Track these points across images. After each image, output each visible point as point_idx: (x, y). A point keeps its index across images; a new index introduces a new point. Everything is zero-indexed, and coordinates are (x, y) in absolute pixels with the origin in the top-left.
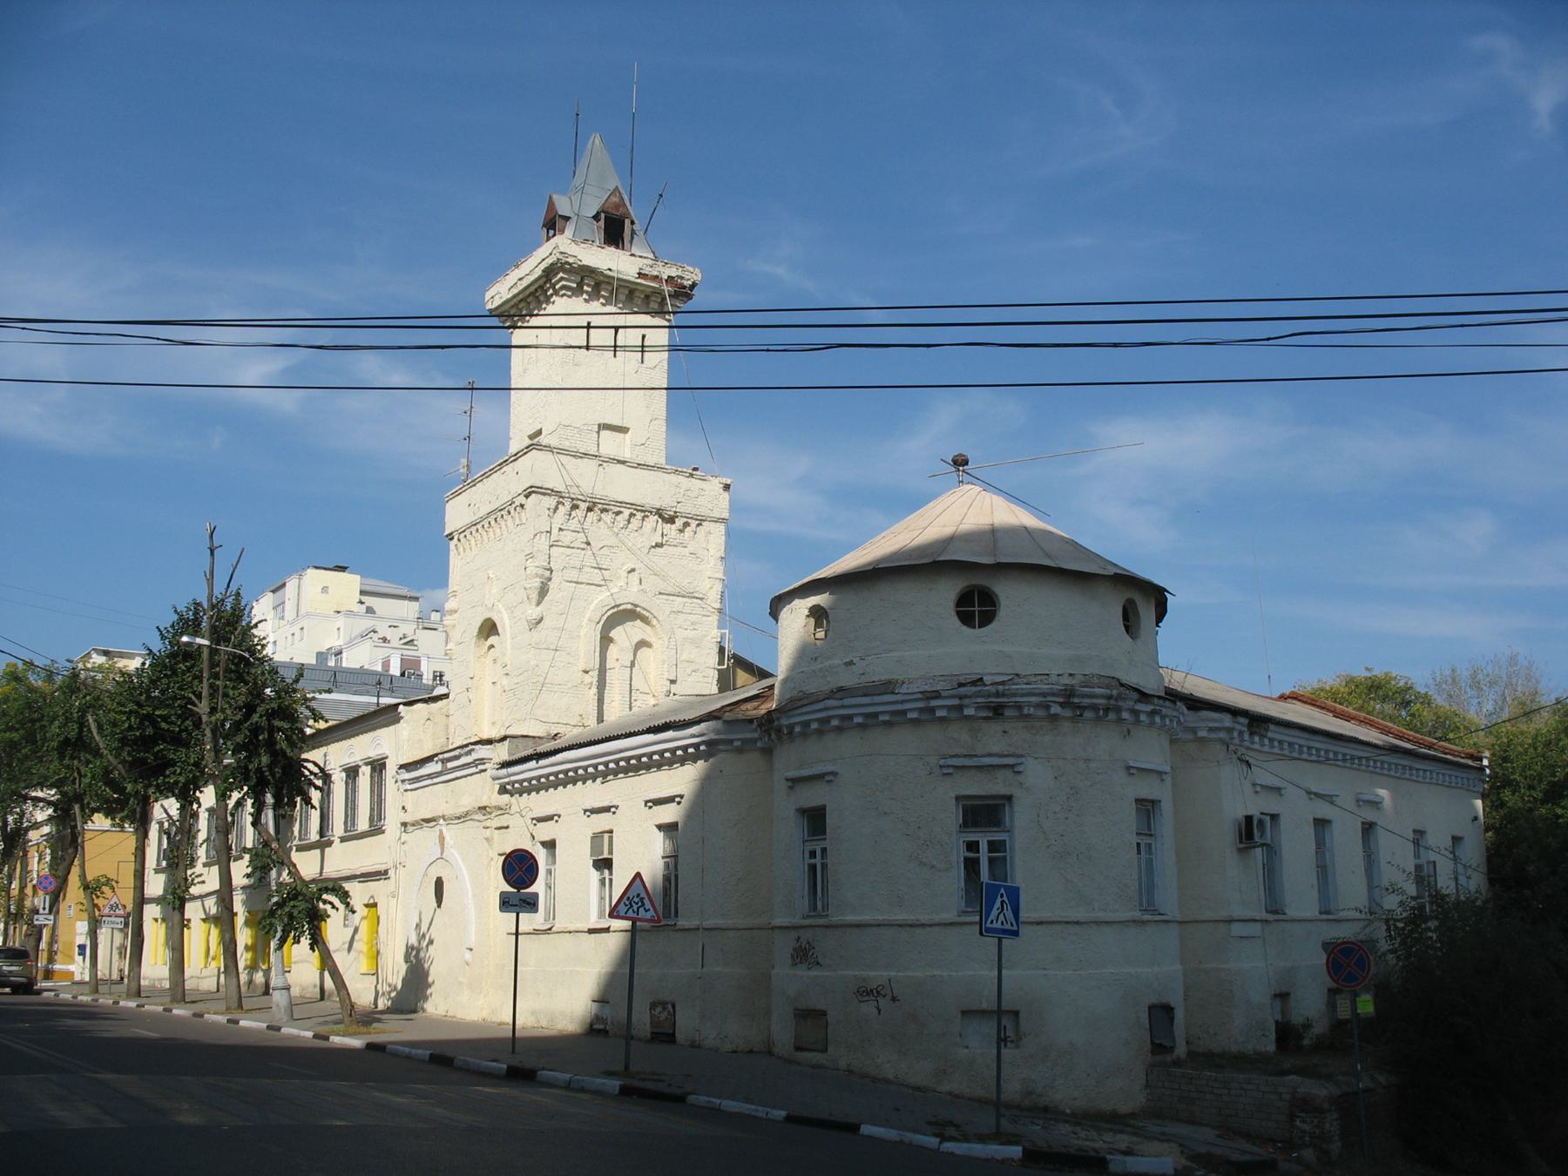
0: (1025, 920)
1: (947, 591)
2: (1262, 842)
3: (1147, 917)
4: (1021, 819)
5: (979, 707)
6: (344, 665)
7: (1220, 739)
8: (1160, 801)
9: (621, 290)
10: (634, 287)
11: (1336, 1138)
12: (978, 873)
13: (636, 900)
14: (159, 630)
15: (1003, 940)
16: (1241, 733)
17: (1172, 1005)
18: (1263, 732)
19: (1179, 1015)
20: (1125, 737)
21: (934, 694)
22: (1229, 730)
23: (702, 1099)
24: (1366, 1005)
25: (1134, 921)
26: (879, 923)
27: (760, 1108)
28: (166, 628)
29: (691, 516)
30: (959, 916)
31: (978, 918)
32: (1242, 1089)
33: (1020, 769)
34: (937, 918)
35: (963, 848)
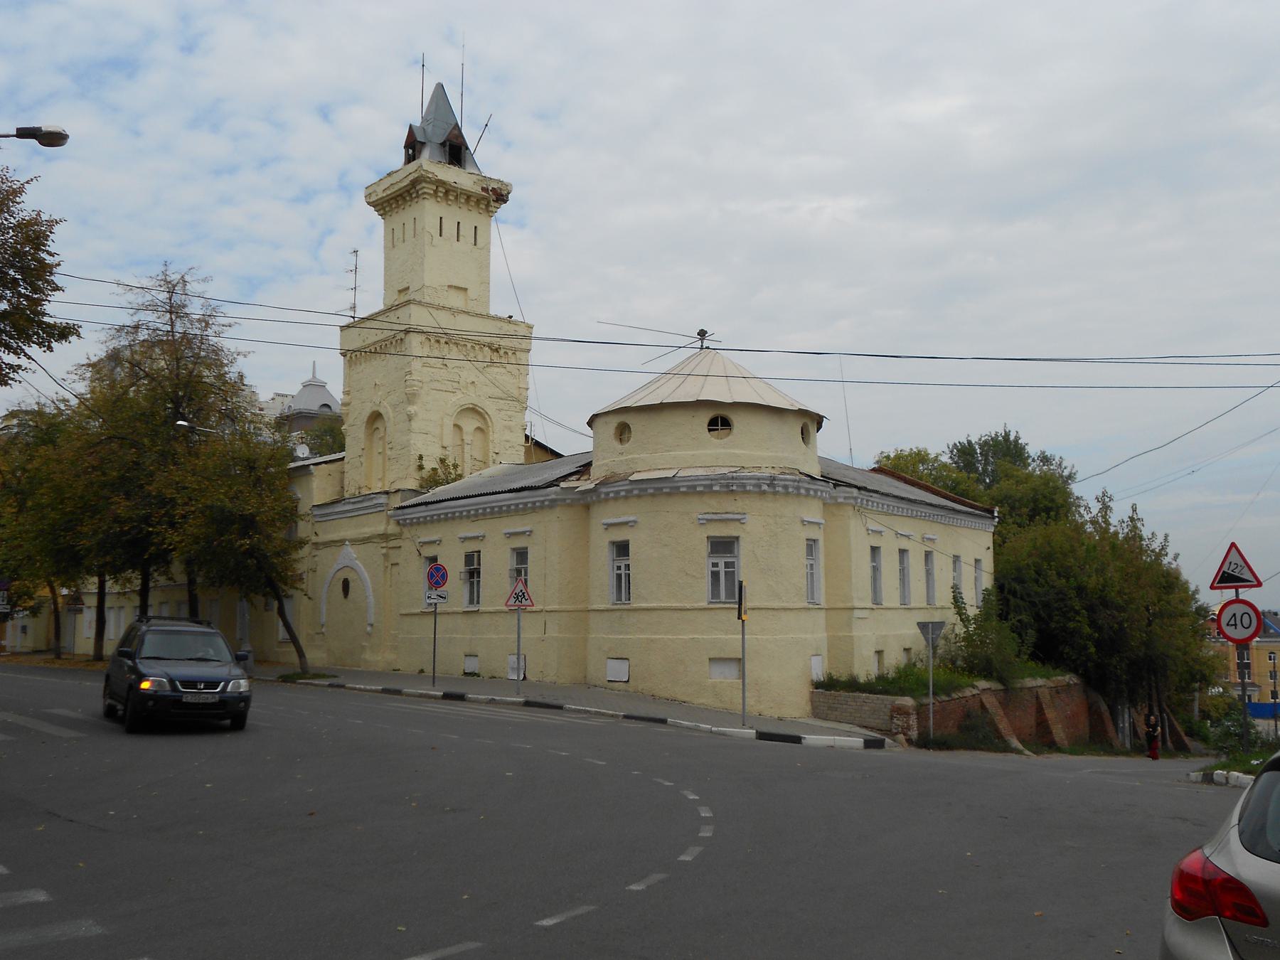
1: (705, 417)
3: (811, 606)
4: (744, 549)
9: (462, 196)
10: (471, 194)
22: (855, 498)
31: (737, 606)
32: (864, 702)
34: (696, 605)
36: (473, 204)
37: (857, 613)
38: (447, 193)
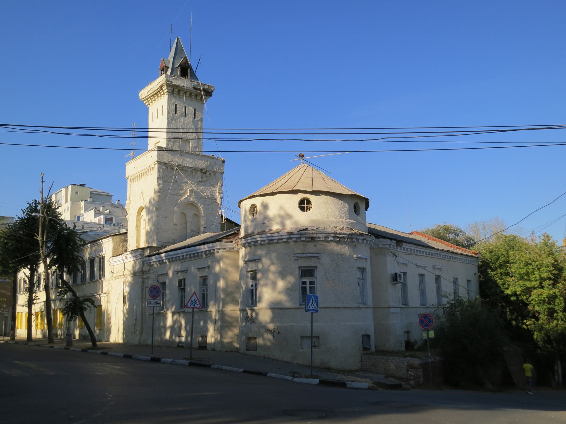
0: (321, 307)
2: (400, 281)
3: (361, 306)
4: (319, 274)
5: (307, 238)
6: (84, 221)
7: (386, 248)
8: (366, 268)
9: (187, 93)
11: (422, 377)
12: (306, 292)
13: (194, 301)
14: (22, 210)
15: (313, 313)
16: (393, 246)
17: (370, 335)
18: (401, 245)
19: (372, 338)
20: (354, 247)
21: (291, 233)
22: (390, 245)
23: (216, 366)
24: (432, 334)
25: (357, 307)
26: (274, 308)
27: (235, 368)
28: (25, 209)
29: (211, 171)
30: (300, 305)
31: (305, 307)
33: (320, 257)
35: (301, 283)
36: (193, 97)
37: (392, 310)
38: (179, 91)
